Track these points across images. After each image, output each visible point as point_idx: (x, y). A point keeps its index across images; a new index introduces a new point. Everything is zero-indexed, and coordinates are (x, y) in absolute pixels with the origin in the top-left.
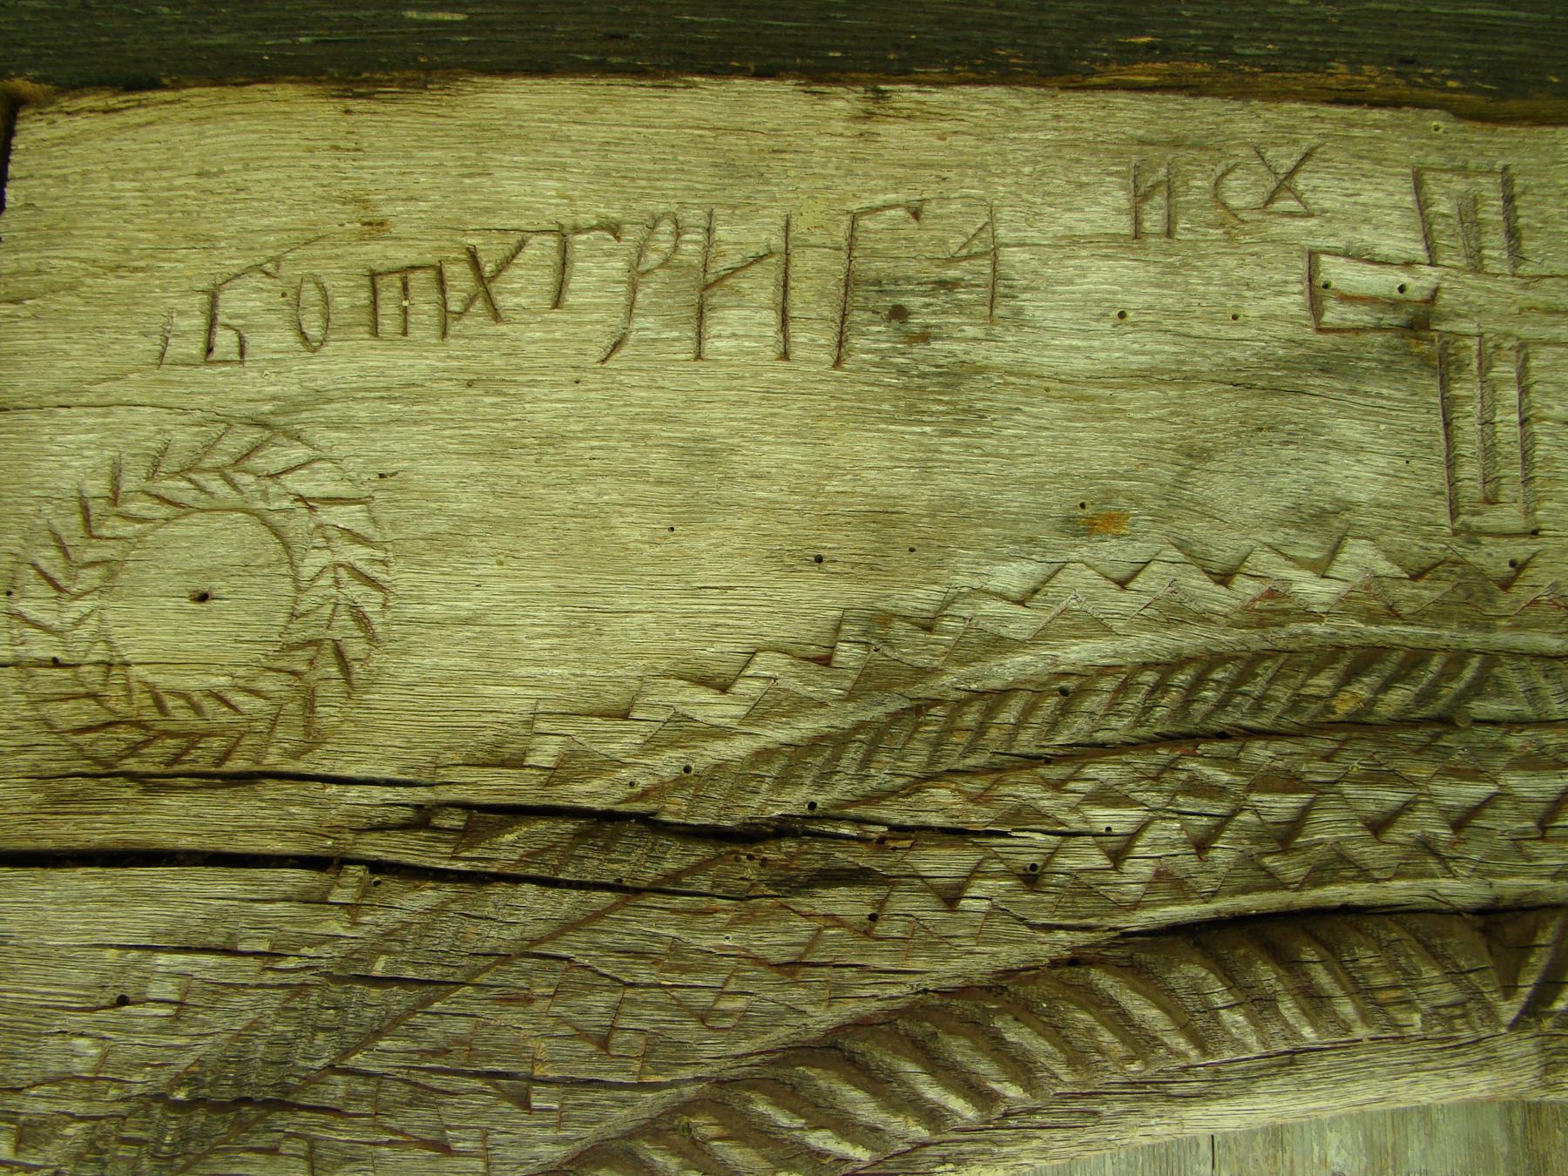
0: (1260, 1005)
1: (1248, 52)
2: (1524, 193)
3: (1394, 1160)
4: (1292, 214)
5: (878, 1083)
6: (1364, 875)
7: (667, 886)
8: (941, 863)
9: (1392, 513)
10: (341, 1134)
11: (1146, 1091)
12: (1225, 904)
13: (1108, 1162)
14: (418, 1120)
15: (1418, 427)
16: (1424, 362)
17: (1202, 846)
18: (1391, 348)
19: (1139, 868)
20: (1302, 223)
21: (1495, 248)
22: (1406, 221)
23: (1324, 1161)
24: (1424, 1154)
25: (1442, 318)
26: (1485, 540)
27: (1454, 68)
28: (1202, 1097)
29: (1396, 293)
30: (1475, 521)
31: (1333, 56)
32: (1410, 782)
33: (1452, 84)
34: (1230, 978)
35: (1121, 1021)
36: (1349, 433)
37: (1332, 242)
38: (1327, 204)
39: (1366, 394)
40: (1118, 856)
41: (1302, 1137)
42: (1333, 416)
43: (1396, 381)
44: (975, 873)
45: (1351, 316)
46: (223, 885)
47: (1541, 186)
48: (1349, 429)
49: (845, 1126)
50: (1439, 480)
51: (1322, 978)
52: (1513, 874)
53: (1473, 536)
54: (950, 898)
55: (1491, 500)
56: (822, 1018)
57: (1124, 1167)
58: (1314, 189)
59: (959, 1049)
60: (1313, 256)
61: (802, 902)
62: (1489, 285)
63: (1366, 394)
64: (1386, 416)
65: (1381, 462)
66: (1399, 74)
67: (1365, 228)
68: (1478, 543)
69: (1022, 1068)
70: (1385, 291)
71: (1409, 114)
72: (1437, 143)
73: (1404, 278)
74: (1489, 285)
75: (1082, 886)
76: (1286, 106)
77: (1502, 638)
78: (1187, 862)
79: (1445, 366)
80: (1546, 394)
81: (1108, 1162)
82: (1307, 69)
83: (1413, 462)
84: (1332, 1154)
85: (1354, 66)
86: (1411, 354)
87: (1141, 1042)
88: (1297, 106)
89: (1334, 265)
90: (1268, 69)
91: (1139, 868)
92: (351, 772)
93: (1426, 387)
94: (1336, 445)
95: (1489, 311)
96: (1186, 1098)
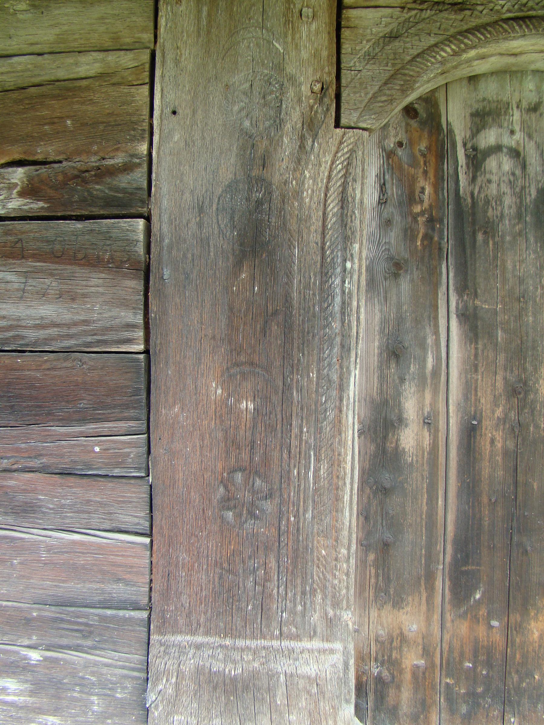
0: (520, 27)
5: (473, 34)
6: (535, 10)
7: (446, 10)
8: (480, 8)
10: (408, 40)
11: (505, 39)
12: (516, 14)
14: (417, 38)
17: (513, 6)
19: (505, 8)
28: (512, 40)
34: (517, 23)
35: (502, 27)
40: (502, 8)
44: (484, 9)
46: (389, 11)
49: (469, 39)
51: (528, 23)
54: (481, 12)
56: (465, 27)
59: (482, 30)
61: (462, 12)
69: (490, 33)
75: (498, 11)
78: (511, 8)
87: (506, 31)
91: (505, 8)
92: (162, 22)
96: (510, 40)
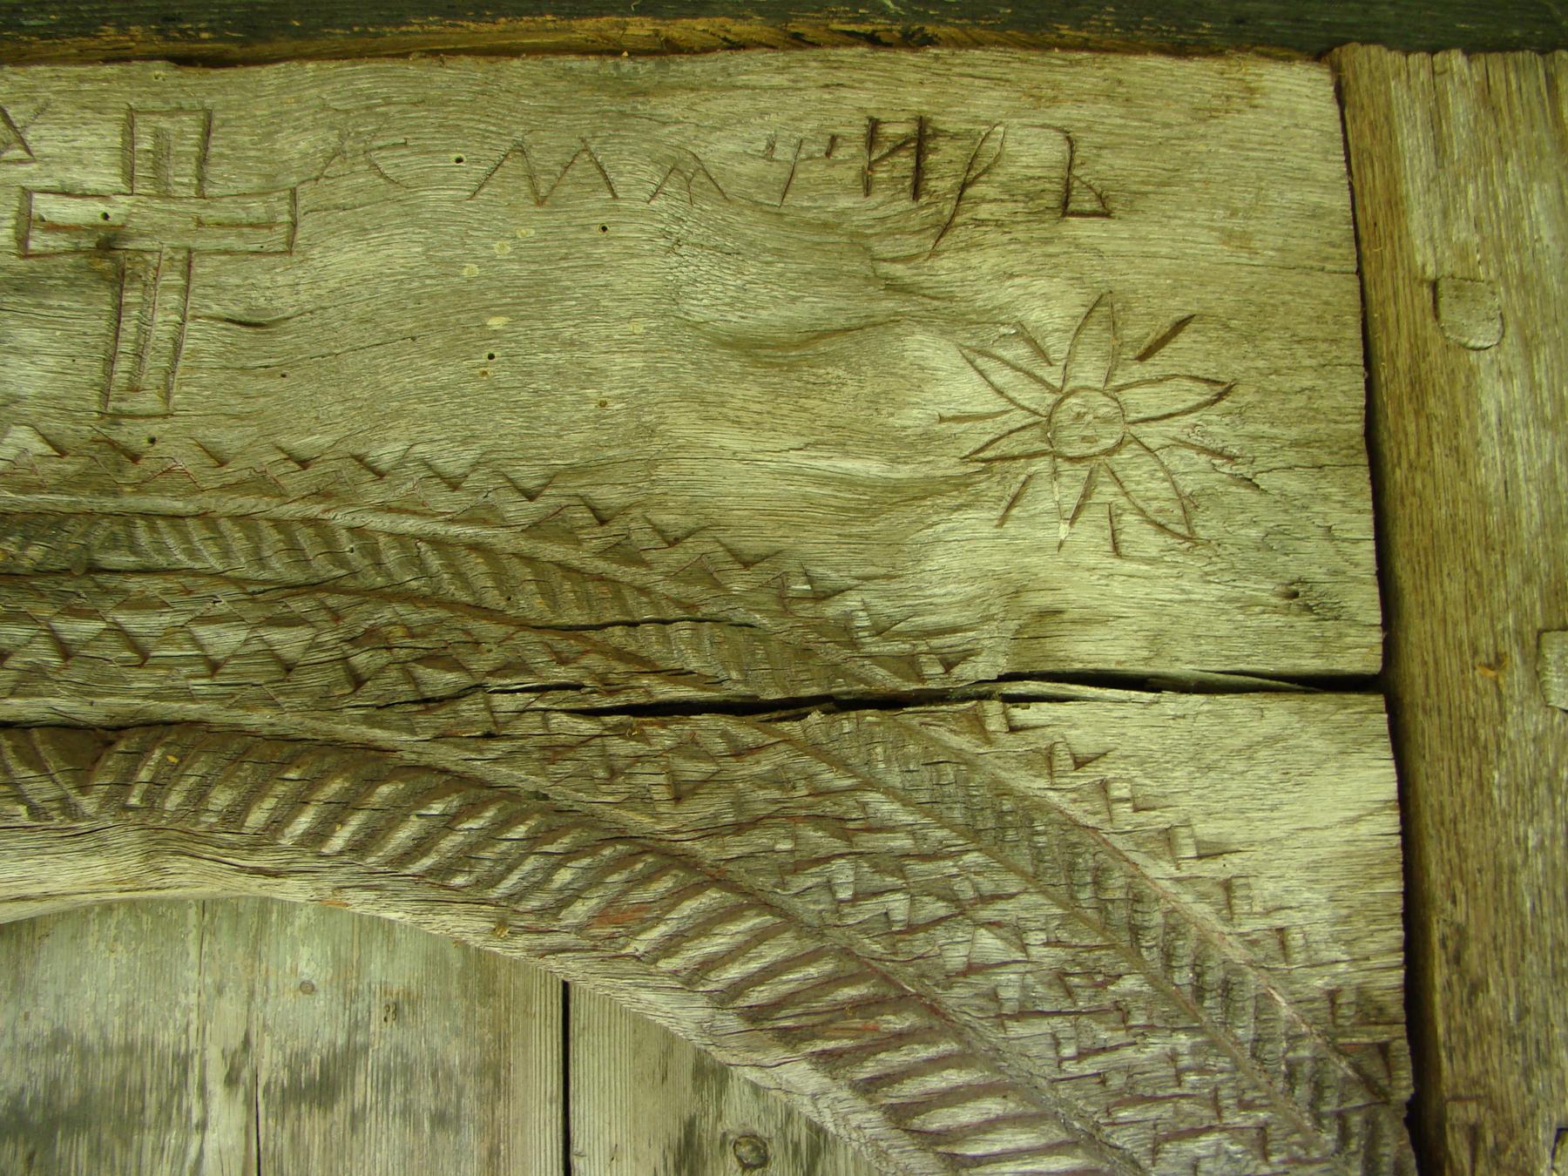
1: (32, 23)
2: (223, 126)
3: (358, 972)
4: (21, 161)
9: (52, 403)
13: (112, 966)
15: (89, 331)
16: (102, 277)
18: (77, 267)
20: (23, 168)
21: (182, 175)
22: (113, 159)
23: (294, 970)
24: (384, 968)
25: (128, 238)
26: (124, 421)
27: (211, 21)
29: (101, 221)
30: (124, 406)
31: (105, 21)
32: (35, 621)
33: (205, 35)
36: (29, 340)
37: (47, 183)
38: (48, 151)
39: (50, 307)
41: (278, 951)
42: (17, 327)
43: (77, 294)
45: (51, 243)
47: (241, 118)
48: (29, 336)
50: (97, 375)
52: (112, 695)
53: (117, 417)
55: (134, 389)
57: (124, 971)
58: (41, 138)
60: (27, 193)
62: (173, 207)
63: (50, 307)
64: (62, 324)
65: (50, 361)
66: (159, 32)
67: (76, 168)
68: (119, 424)
70: (90, 220)
71: (136, 67)
72: (154, 89)
73: (103, 207)
74: (173, 207)
76: (33, 69)
77: (131, 502)
79: (118, 280)
80: (205, 297)
81: (112, 966)
82: (80, 34)
83: (79, 361)
84: (302, 965)
85: (122, 27)
86: (94, 271)
88: (40, 68)
89: (44, 202)
90: (43, 37)
93: (100, 298)
94: (16, 351)
95: (171, 230)
